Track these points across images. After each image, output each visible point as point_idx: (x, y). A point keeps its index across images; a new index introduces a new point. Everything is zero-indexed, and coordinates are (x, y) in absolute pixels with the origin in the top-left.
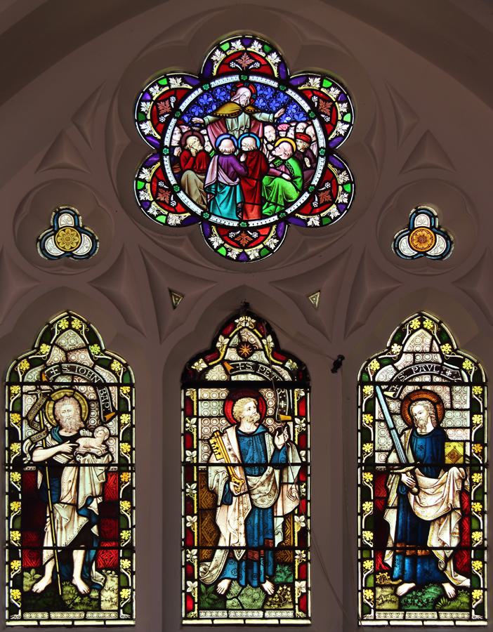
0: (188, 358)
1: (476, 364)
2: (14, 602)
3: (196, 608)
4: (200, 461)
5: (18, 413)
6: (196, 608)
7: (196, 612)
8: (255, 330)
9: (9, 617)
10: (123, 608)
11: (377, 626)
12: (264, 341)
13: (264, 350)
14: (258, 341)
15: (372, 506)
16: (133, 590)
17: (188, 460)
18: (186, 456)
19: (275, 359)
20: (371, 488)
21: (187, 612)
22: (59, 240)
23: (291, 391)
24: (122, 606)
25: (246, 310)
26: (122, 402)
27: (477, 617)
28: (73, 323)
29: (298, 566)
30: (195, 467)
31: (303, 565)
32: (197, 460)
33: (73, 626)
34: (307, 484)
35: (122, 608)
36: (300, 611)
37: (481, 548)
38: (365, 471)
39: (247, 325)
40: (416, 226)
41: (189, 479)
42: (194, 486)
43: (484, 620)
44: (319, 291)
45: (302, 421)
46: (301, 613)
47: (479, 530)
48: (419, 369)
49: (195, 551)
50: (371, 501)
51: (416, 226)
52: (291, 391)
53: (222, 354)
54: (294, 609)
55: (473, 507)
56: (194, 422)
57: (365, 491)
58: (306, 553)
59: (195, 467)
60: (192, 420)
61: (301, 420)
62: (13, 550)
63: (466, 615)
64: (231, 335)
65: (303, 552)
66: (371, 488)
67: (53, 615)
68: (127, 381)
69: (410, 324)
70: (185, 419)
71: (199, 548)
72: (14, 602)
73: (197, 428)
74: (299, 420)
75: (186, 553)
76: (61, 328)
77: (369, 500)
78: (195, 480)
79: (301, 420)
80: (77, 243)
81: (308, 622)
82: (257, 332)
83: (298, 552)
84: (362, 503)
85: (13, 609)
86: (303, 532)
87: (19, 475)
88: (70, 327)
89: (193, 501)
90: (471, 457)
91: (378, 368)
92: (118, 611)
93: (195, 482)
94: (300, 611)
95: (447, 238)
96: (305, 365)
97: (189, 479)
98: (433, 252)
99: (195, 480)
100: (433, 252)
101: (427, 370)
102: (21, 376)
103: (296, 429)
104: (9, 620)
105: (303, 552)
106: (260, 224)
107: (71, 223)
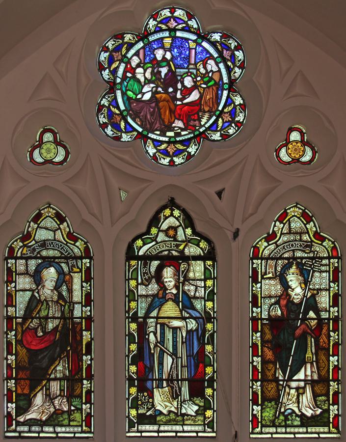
0: (130, 239)
1: (333, 243)
2: (132, 418)
3: (260, 425)
4: (17, 316)
5: (135, 279)
6: (260, 425)
7: (259, 428)
8: (301, 218)
9: (129, 430)
10: (207, 424)
11: (258, 438)
12: (308, 226)
13: (308, 233)
14: (303, 226)
15: (136, 347)
16: (214, 411)
17: (254, 315)
18: (253, 312)
19: (316, 239)
20: (136, 335)
21: (253, 429)
22: (52, 155)
23: (140, 262)
24: (206, 423)
25: (172, 204)
26: (208, 272)
27: (209, 430)
28: (174, 212)
29: (333, 395)
30: (14, 320)
31: (336, 394)
32: (261, 315)
33: (74, 437)
34: (338, 333)
35: (206, 424)
36: (333, 428)
37: (211, 381)
38: (131, 322)
39: (50, 214)
40: (291, 140)
41: (255, 330)
42: (13, 333)
43: (213, 432)
44: (120, 190)
45: (88, 285)
46: (333, 429)
47: (210, 365)
48: (160, 248)
49: (259, 383)
50: (135, 343)
51: (291, 140)
52: (140, 262)
53: (33, 236)
54: (81, 426)
55: (206, 348)
56: (14, 286)
57: (131, 335)
58: (338, 384)
59: (14, 320)
60: (12, 284)
61: (87, 284)
62: (131, 380)
63: (326, 429)
64: (284, 222)
65: (335, 384)
66: (136, 335)
67: (309, 430)
68: (335, 254)
69: (164, 213)
70: (252, 284)
71: (262, 381)
72: (132, 418)
73: (261, 291)
74: (333, 284)
75: (7, 383)
76: (165, 216)
77: (134, 343)
78: (260, 330)
79: (87, 284)
80: (290, 154)
81: (214, 435)
82: (303, 220)
83: (331, 383)
84: (129, 345)
85: (131, 425)
86: (336, 368)
87: (136, 324)
88: (172, 215)
89: (13, 344)
90: (205, 312)
91: (142, 245)
92: (204, 425)
93: (14, 330)
94: (333, 428)
95: (313, 149)
96: (213, 243)
97: (255, 330)
98: (303, 159)
99: (260, 330)
100: (57, 160)
101: (59, 248)
102: (136, 251)
103: (83, 291)
104: (129, 432)
105: (335, 384)
106: (158, 139)
107: (51, 139)
